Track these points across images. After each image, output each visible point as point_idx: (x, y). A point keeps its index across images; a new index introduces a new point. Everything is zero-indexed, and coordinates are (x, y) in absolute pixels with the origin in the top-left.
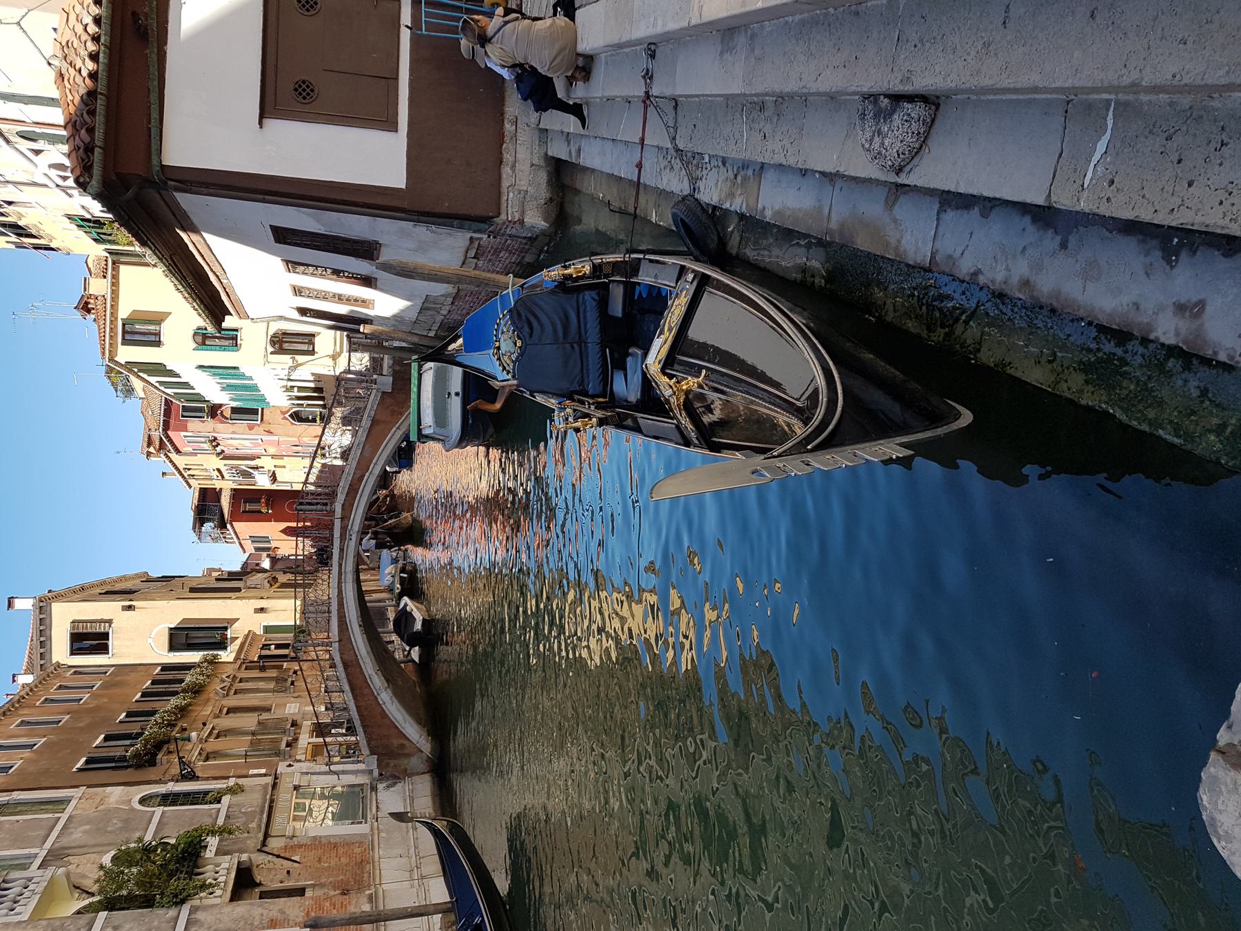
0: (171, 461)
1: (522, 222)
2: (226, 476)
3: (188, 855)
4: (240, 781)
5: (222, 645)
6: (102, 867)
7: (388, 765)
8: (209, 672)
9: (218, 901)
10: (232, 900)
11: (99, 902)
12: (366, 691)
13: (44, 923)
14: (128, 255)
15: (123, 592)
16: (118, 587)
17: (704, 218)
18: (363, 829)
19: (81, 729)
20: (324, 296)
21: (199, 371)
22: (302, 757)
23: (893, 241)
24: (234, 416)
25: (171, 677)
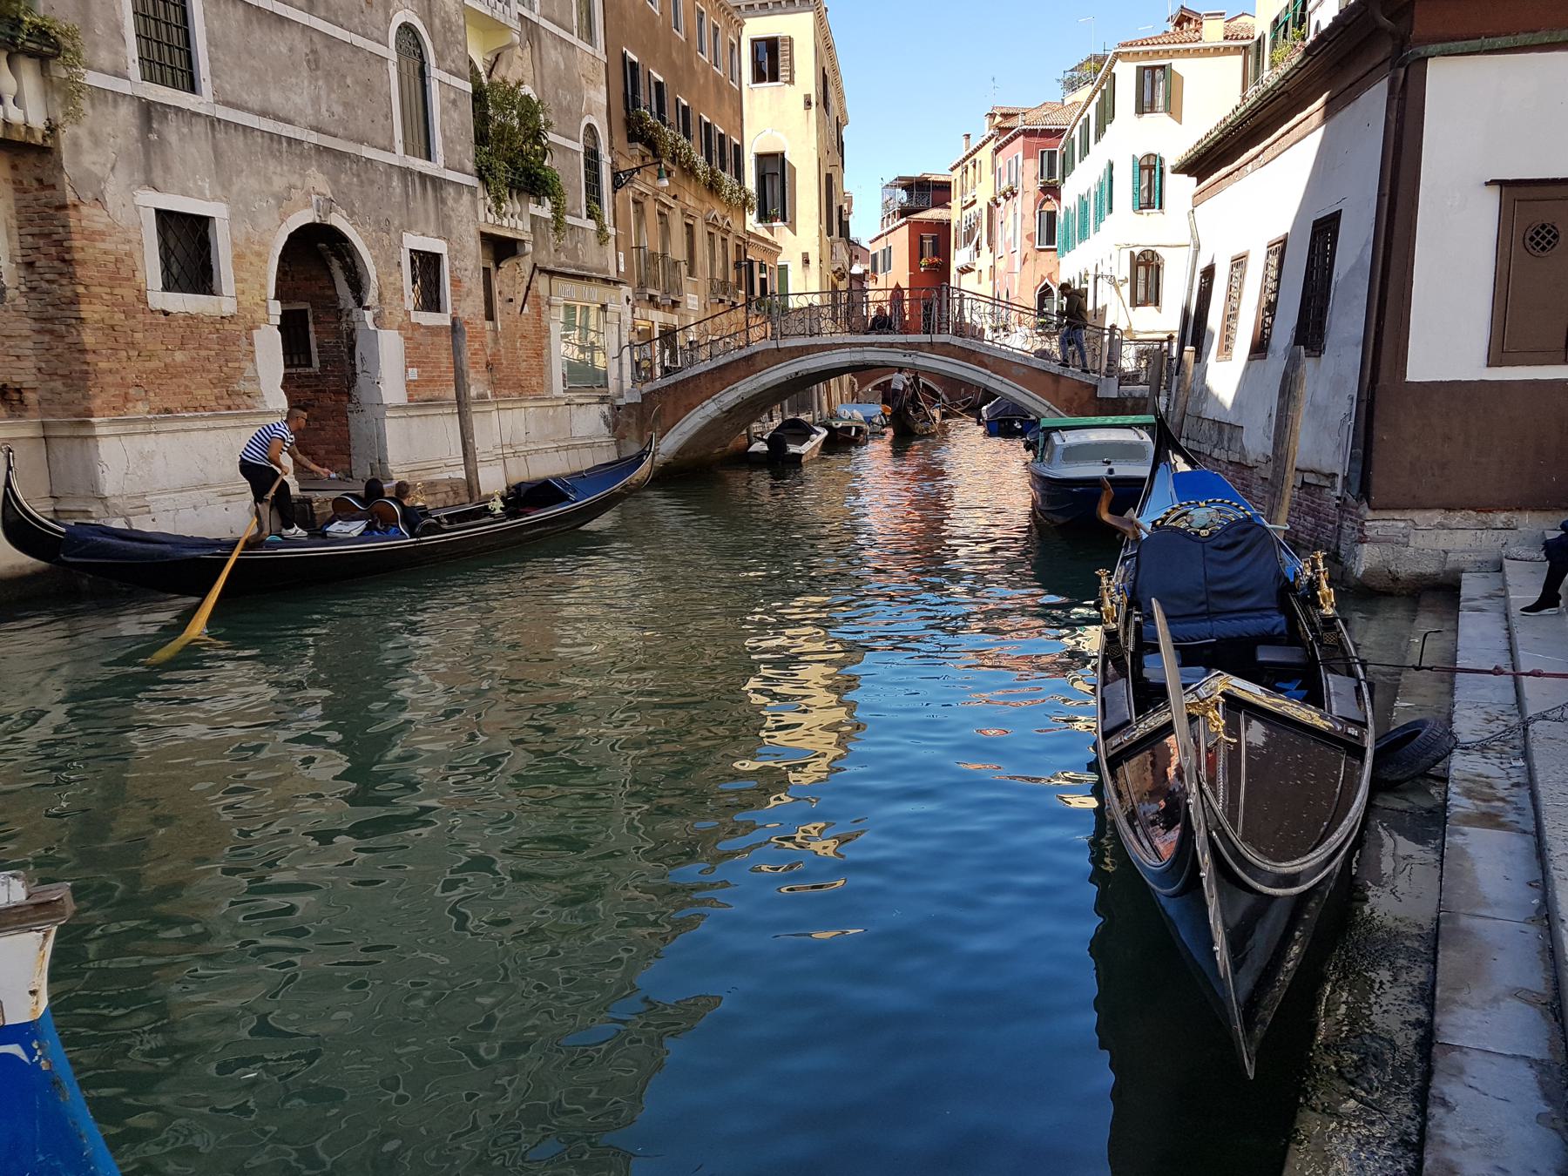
0: (984, 143)
1: (1362, 540)
3: (533, 182)
4: (612, 240)
5: (764, 217)
6: (520, 83)
7: (630, 416)
8: (734, 201)
9: (482, 219)
10: (482, 234)
11: (481, 84)
12: (718, 384)
13: (461, 22)
14: (1257, 63)
15: (826, 96)
16: (831, 89)
17: (1424, 761)
18: (558, 387)
19: (670, 54)
20: (1233, 296)
21: (1105, 165)
22: (637, 315)
23: (1463, 996)
24: (1044, 216)
25: (728, 156)
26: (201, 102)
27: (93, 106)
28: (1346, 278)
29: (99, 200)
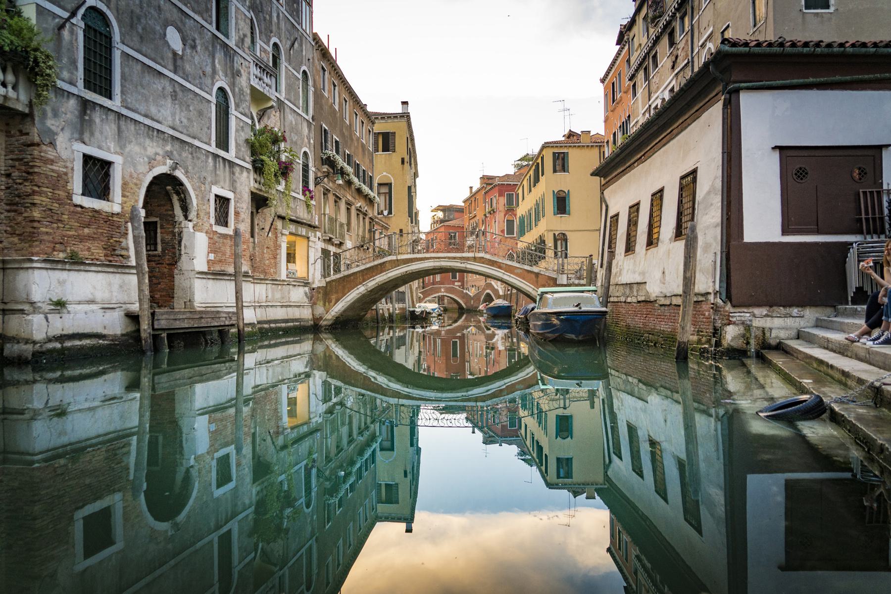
2: (471, 221)
12: (366, 277)
26: (115, 104)
27: (56, 97)
28: (704, 198)
29: (52, 144)
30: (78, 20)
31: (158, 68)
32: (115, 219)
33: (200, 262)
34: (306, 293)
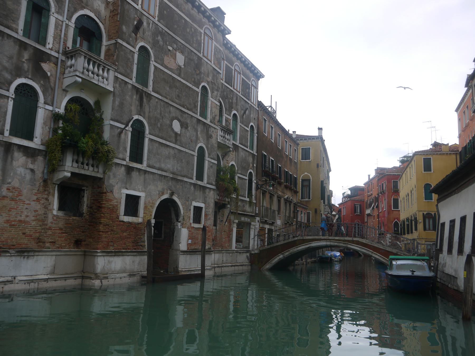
2: (369, 198)
29: (112, 192)
30: (129, 128)
31: (168, 143)
32: (139, 226)
33: (183, 246)
34: (247, 257)
